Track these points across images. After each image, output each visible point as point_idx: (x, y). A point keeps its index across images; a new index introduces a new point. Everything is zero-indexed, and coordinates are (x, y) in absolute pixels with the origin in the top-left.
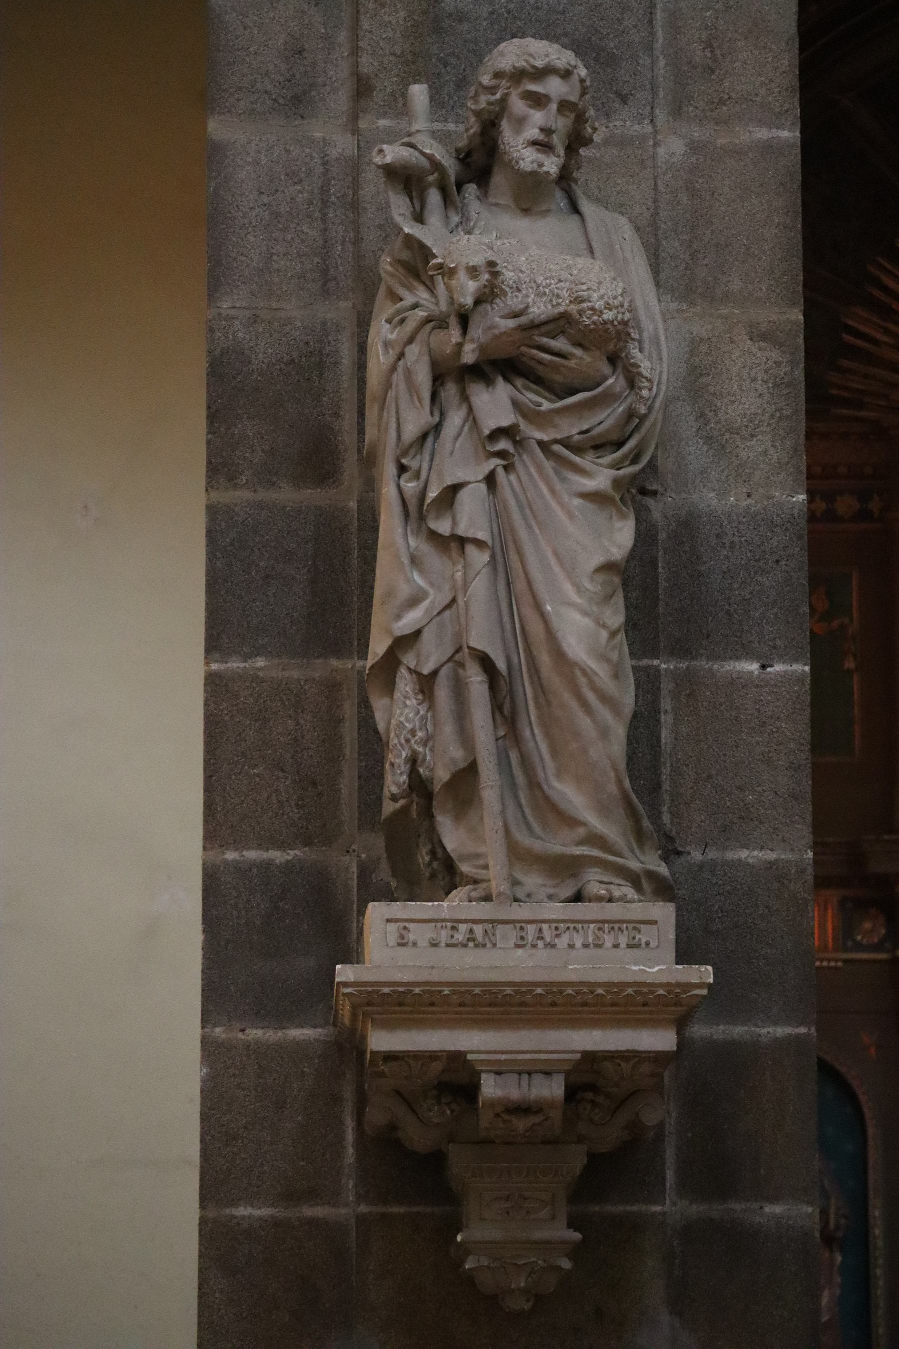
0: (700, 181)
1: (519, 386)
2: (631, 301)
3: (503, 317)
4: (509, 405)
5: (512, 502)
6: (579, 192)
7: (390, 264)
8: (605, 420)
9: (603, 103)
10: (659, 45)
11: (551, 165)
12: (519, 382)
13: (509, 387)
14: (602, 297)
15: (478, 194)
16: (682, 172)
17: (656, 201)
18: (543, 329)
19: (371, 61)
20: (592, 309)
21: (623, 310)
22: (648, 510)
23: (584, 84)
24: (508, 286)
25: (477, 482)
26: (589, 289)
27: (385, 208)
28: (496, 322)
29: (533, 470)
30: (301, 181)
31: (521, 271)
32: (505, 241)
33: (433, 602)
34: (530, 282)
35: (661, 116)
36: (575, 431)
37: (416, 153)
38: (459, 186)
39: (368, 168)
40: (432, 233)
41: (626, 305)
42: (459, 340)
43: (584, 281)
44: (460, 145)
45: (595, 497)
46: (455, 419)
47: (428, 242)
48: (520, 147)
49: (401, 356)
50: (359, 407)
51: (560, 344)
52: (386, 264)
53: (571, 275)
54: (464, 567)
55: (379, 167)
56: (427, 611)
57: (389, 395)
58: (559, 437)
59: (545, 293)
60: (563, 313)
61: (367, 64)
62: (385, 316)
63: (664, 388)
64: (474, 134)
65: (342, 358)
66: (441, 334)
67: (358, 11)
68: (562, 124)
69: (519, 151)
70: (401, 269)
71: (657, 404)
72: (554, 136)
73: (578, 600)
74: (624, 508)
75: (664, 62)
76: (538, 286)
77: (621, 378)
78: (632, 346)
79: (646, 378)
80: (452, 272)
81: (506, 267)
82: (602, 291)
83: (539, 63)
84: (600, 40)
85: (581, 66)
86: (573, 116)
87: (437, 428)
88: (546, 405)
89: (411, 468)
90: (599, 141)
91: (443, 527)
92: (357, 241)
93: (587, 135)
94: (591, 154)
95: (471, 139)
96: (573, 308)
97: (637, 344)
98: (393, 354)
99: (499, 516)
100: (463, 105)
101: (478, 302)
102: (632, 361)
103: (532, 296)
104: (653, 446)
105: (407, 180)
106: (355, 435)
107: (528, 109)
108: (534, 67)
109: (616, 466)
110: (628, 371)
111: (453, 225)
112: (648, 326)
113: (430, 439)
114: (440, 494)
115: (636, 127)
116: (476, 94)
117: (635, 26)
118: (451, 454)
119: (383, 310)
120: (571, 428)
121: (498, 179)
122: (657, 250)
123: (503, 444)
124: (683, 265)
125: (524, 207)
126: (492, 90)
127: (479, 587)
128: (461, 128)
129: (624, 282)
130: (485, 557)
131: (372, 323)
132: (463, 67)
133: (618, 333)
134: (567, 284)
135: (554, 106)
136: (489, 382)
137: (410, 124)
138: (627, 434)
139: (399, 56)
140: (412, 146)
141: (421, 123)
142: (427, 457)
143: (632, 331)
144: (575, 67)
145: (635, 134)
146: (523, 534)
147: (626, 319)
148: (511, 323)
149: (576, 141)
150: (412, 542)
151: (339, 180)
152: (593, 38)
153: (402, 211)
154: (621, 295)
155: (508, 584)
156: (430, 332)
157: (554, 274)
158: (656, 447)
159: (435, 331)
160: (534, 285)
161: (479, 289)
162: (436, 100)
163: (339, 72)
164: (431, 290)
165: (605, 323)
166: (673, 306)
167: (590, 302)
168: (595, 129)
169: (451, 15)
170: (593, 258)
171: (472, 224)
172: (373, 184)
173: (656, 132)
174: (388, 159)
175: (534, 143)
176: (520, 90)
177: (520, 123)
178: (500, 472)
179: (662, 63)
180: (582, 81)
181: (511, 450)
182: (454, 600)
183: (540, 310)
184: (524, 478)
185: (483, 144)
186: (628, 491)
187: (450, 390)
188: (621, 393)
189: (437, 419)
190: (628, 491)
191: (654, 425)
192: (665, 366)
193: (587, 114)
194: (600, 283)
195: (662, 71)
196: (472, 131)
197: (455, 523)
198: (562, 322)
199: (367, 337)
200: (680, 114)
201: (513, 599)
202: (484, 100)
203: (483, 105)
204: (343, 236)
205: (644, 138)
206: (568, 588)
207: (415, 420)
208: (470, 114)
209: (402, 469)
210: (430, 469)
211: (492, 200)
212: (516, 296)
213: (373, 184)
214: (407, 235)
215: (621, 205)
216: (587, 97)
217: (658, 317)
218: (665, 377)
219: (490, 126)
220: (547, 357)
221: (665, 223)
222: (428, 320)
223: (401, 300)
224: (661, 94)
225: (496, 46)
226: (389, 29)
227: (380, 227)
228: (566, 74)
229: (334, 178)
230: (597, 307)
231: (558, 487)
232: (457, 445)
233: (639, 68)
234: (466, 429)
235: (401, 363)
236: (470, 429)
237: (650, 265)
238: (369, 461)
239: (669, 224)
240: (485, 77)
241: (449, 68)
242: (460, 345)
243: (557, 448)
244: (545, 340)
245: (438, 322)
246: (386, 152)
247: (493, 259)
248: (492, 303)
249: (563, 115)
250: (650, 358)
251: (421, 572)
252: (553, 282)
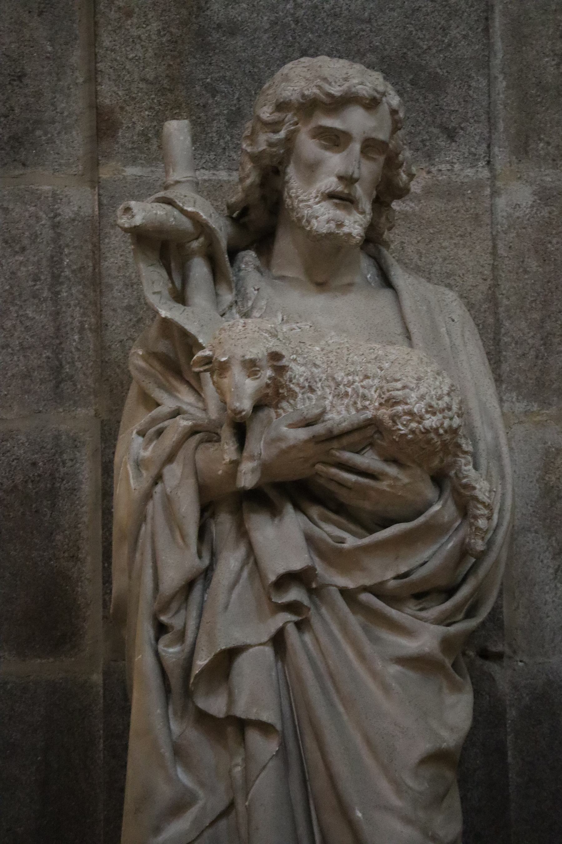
0: (554, 241)
1: (315, 517)
2: (461, 402)
3: (290, 426)
4: (302, 542)
5: (308, 672)
6: (390, 258)
7: (142, 357)
8: (429, 559)
9: (423, 141)
10: (498, 62)
11: (354, 225)
12: (315, 511)
13: (301, 519)
14: (422, 397)
15: (258, 263)
16: (530, 230)
17: (494, 268)
18: (345, 441)
19: (115, 89)
20: (410, 413)
21: (450, 413)
22: (492, 679)
23: (396, 117)
24: (298, 384)
25: (261, 644)
26: (404, 387)
27: (134, 284)
28: (283, 431)
29: (335, 628)
30: (23, 249)
31: (315, 365)
32: (294, 326)
33: (204, 808)
34: (327, 379)
35: (501, 156)
36: (390, 575)
37: (176, 213)
38: (233, 253)
39: (112, 232)
40: (198, 316)
41: (455, 407)
42: (234, 457)
43: (398, 376)
44: (233, 200)
45: (417, 663)
46: (231, 561)
47: (192, 328)
48: (312, 201)
49: (158, 479)
50: (104, 547)
51: (368, 460)
52: (137, 359)
53: (381, 369)
54: (246, 760)
55: (126, 230)
56: (196, 821)
57: (143, 528)
58: (368, 582)
59: (346, 394)
60: (371, 419)
61: (109, 93)
62: (137, 426)
63: (507, 516)
64: (251, 185)
65: (81, 483)
66: (212, 449)
67: (96, 23)
68: (368, 170)
69: (310, 206)
70: (156, 364)
71: (500, 538)
72: (357, 185)
73: (396, 801)
74: (458, 678)
75: (504, 83)
76: (338, 384)
77: (450, 503)
78: (463, 461)
79: (483, 503)
80: (223, 368)
81: (295, 360)
82: (423, 390)
83: (336, 90)
84: (419, 56)
85: (392, 93)
86: (382, 159)
87: (207, 574)
88: (351, 542)
89: (172, 627)
90: (418, 191)
91: (216, 706)
92: (100, 328)
93: (401, 185)
94: (408, 208)
95: (248, 192)
96: (385, 413)
97: (470, 458)
98: (147, 476)
99: (290, 689)
100: (238, 147)
101: (258, 407)
102: (464, 481)
103: (330, 397)
104: (495, 593)
105: (162, 247)
106: (100, 585)
107: (323, 151)
108: (329, 95)
109: (446, 620)
110: (459, 494)
111: (225, 305)
112: (485, 435)
113: (198, 587)
114: (211, 662)
115: (470, 172)
116: (254, 132)
117: (465, 37)
118: (226, 607)
119: (135, 419)
120: (384, 571)
121: (285, 244)
122: (497, 333)
123: (294, 594)
124: (533, 353)
125: (320, 281)
126: (274, 126)
127: (266, 787)
128: (235, 176)
129: (451, 377)
130: (273, 746)
131: (120, 437)
132: (237, 96)
133: (445, 444)
134: (376, 381)
135: (356, 147)
136: (275, 512)
137: (167, 172)
138: (460, 578)
139: (151, 83)
140: (169, 202)
141: (180, 172)
142: (194, 613)
143: (463, 442)
144: (384, 94)
145: (466, 180)
146: (321, 711)
147: (455, 426)
148: (302, 434)
149: (387, 192)
150: (175, 727)
151: (75, 248)
152: (410, 54)
153: (157, 289)
154: (448, 394)
155: (304, 782)
156: (196, 448)
157: (358, 368)
158: (501, 593)
159: (202, 446)
160: (332, 384)
161: (258, 390)
162: (200, 140)
163: (75, 104)
164: (198, 391)
165: (427, 431)
166: (520, 407)
167: (406, 404)
168: (411, 176)
169: (219, 26)
170: (411, 346)
171: (250, 304)
172: (118, 252)
173: (494, 177)
174: (138, 220)
175: (331, 196)
176: (312, 124)
177: (312, 169)
178: (291, 630)
179: (501, 84)
180: (394, 112)
181: (306, 601)
182: (231, 806)
183: (340, 416)
184: (324, 639)
185: (263, 198)
186: (464, 654)
187: (224, 524)
188: (452, 522)
189: (206, 561)
190: (464, 654)
191: (496, 563)
192: (509, 487)
193: (401, 157)
194: (419, 379)
195: (501, 96)
196: (248, 181)
197: (231, 702)
198: (370, 431)
199: (114, 453)
200: (526, 152)
201: (311, 802)
202: (263, 139)
203: (263, 146)
204: (81, 322)
205: (479, 185)
206: (384, 786)
207: (178, 563)
208: (246, 159)
209: (161, 629)
210: (198, 628)
211: (275, 271)
212: (309, 398)
213: (118, 252)
214: (165, 321)
215: (449, 275)
216: (400, 133)
217: (500, 425)
218: (509, 502)
219: (272, 174)
220: (352, 478)
221: (508, 298)
222: (193, 432)
223: (158, 405)
224: (501, 126)
225: (280, 66)
226: (138, 46)
227: (129, 308)
228: (372, 104)
229: (67, 246)
230: (415, 410)
231: (369, 648)
232: (234, 596)
233: (471, 92)
234: (245, 574)
235: (158, 488)
236: (250, 575)
237: (488, 353)
238: (118, 618)
239: (513, 298)
240: (265, 109)
241: (218, 98)
242: (236, 464)
243: (365, 597)
244: (347, 456)
245: (206, 434)
246: (135, 211)
247: (277, 349)
248: (276, 407)
249: (369, 158)
250: (489, 478)
251: (189, 767)
252: (357, 378)
